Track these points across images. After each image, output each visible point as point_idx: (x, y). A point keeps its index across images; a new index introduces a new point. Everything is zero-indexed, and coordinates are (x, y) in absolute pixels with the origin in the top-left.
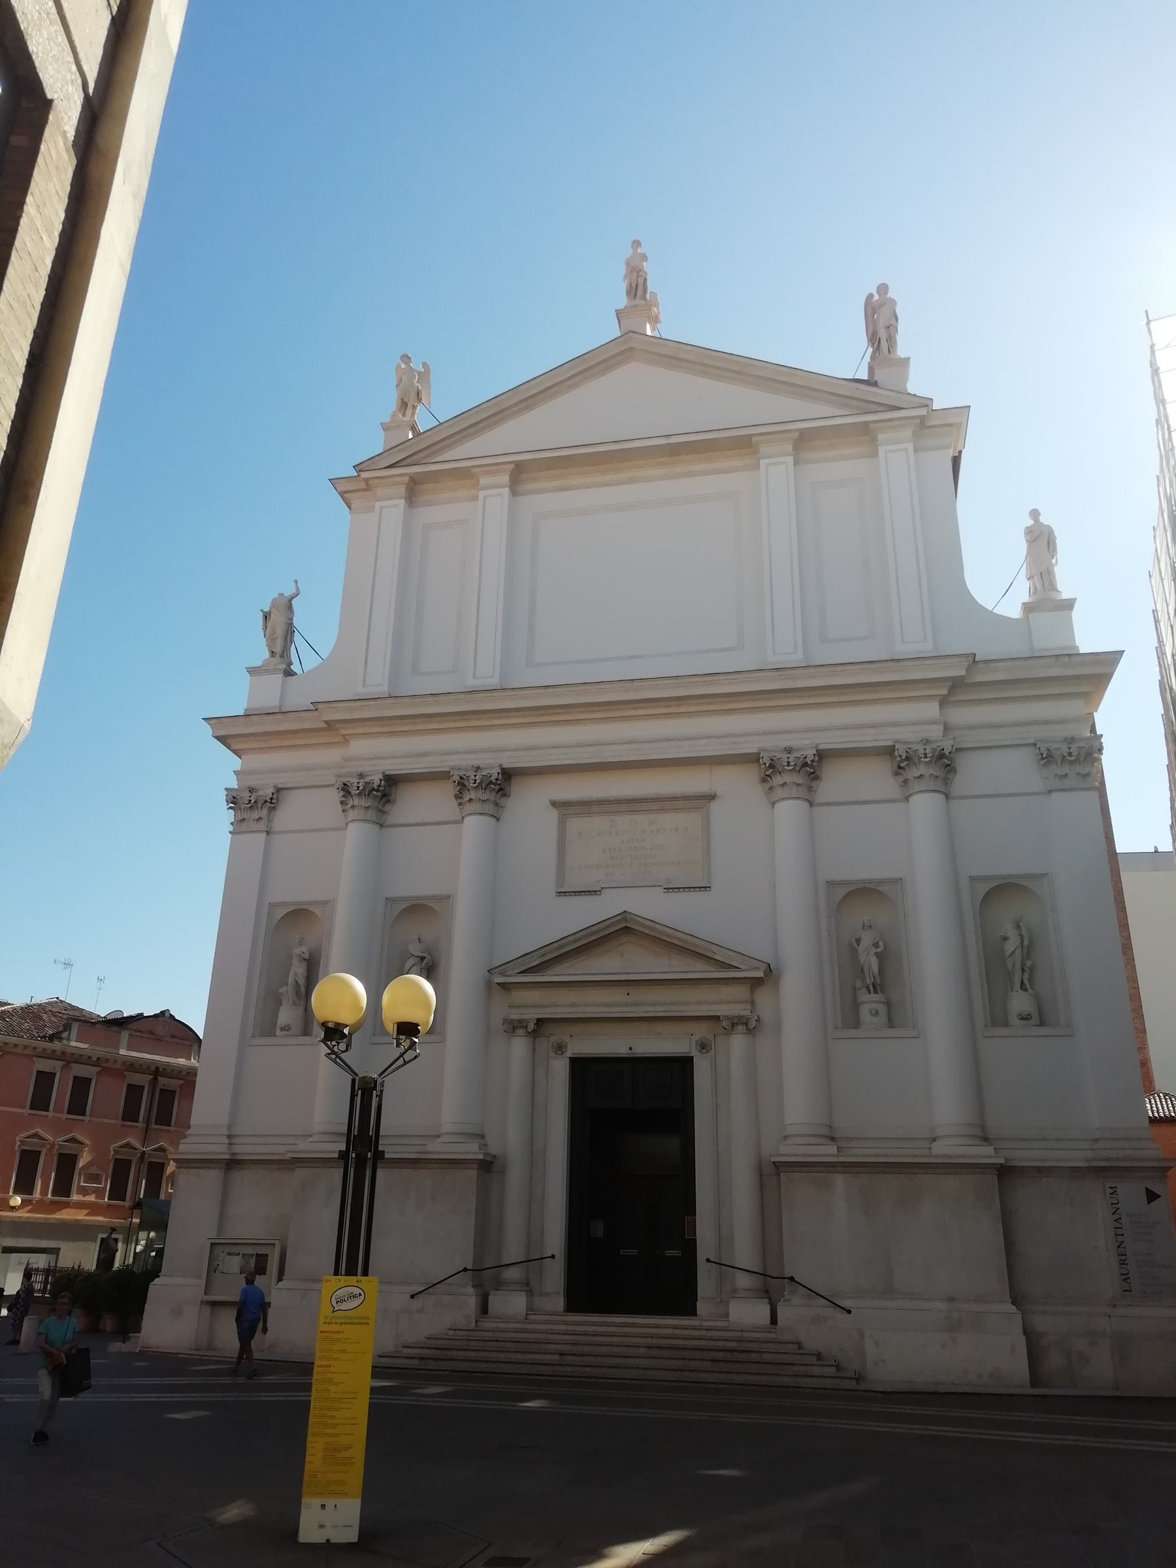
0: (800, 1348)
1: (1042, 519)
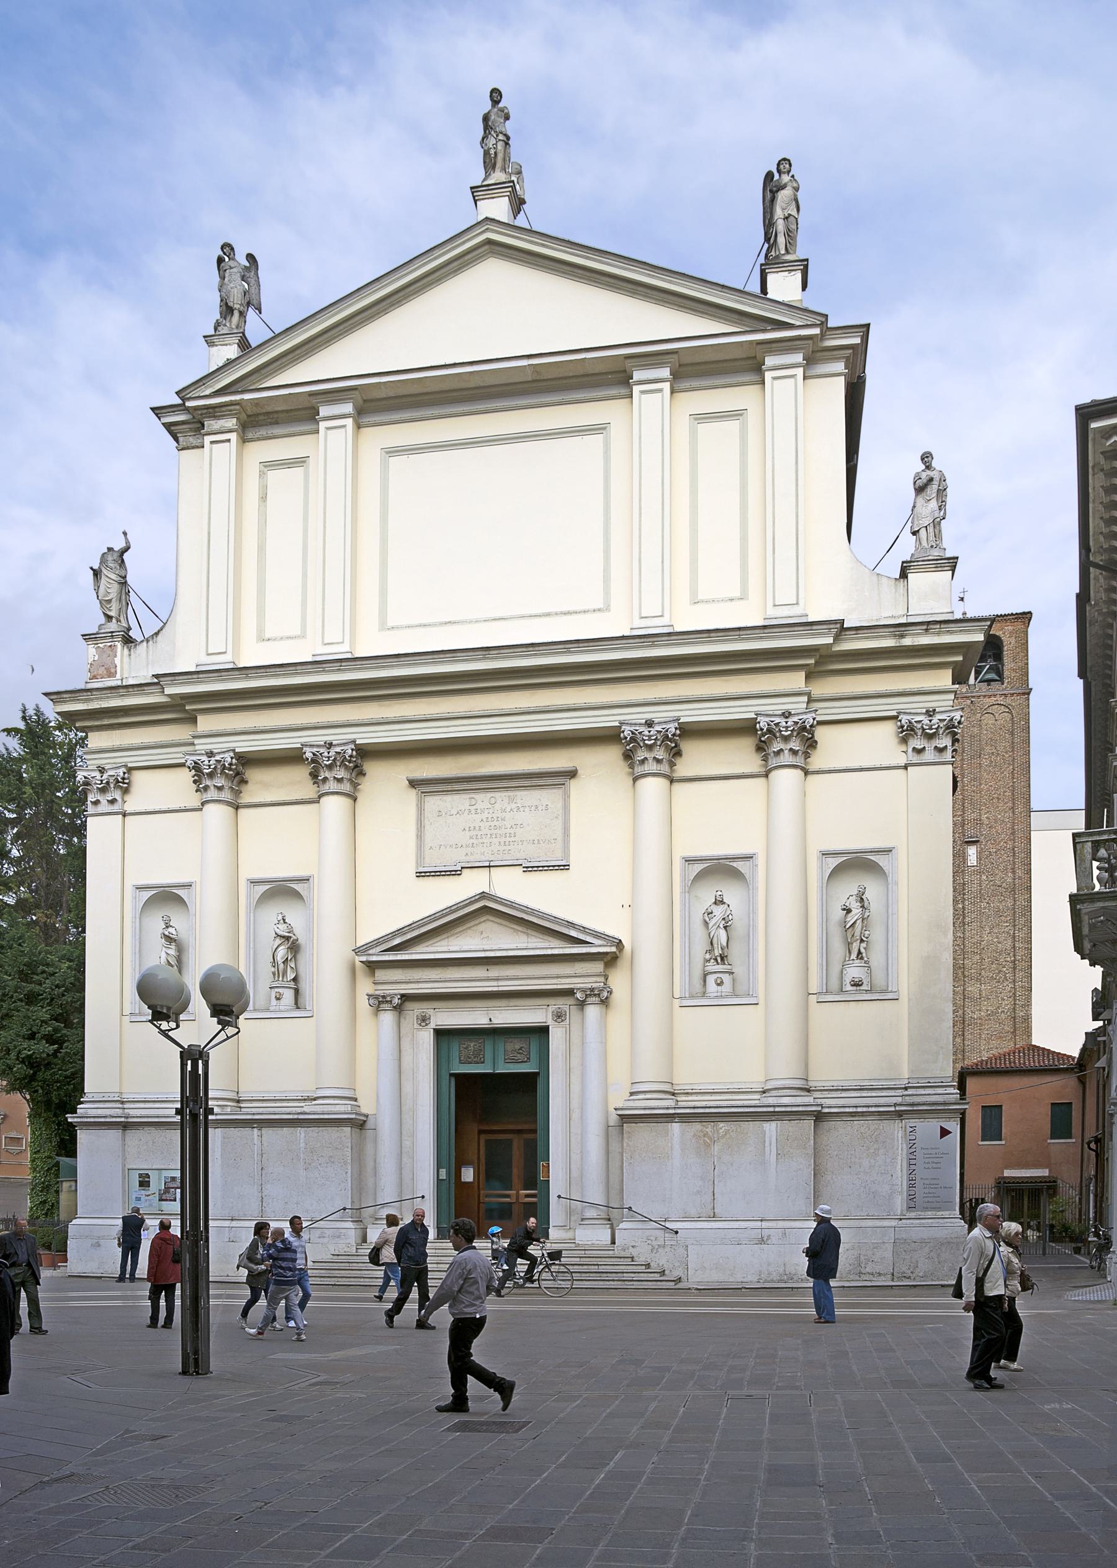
0: (633, 1261)
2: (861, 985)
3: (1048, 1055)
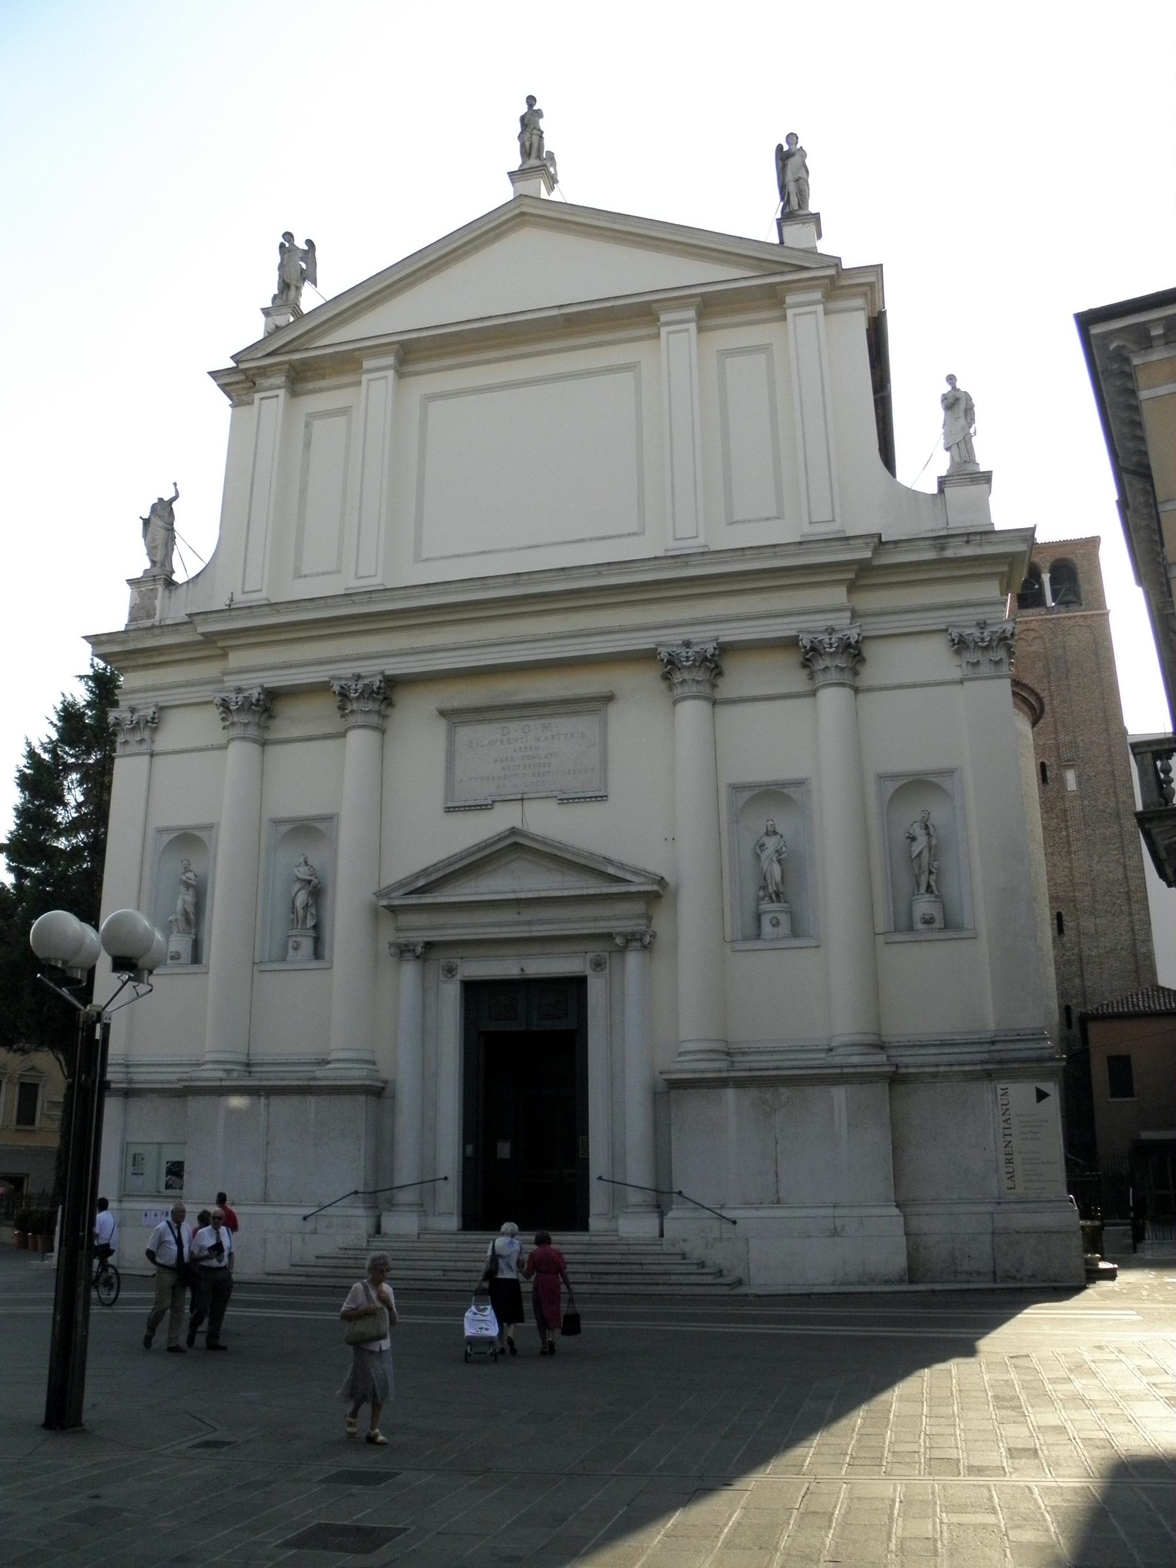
0: (684, 1258)
1: (960, 385)
2: (933, 922)
3: (1169, 996)
